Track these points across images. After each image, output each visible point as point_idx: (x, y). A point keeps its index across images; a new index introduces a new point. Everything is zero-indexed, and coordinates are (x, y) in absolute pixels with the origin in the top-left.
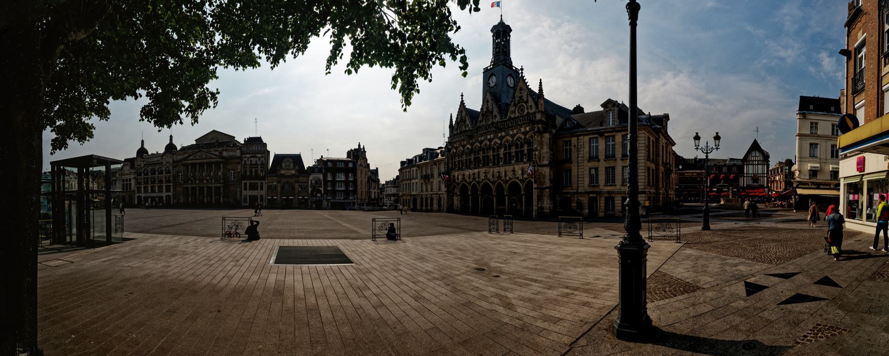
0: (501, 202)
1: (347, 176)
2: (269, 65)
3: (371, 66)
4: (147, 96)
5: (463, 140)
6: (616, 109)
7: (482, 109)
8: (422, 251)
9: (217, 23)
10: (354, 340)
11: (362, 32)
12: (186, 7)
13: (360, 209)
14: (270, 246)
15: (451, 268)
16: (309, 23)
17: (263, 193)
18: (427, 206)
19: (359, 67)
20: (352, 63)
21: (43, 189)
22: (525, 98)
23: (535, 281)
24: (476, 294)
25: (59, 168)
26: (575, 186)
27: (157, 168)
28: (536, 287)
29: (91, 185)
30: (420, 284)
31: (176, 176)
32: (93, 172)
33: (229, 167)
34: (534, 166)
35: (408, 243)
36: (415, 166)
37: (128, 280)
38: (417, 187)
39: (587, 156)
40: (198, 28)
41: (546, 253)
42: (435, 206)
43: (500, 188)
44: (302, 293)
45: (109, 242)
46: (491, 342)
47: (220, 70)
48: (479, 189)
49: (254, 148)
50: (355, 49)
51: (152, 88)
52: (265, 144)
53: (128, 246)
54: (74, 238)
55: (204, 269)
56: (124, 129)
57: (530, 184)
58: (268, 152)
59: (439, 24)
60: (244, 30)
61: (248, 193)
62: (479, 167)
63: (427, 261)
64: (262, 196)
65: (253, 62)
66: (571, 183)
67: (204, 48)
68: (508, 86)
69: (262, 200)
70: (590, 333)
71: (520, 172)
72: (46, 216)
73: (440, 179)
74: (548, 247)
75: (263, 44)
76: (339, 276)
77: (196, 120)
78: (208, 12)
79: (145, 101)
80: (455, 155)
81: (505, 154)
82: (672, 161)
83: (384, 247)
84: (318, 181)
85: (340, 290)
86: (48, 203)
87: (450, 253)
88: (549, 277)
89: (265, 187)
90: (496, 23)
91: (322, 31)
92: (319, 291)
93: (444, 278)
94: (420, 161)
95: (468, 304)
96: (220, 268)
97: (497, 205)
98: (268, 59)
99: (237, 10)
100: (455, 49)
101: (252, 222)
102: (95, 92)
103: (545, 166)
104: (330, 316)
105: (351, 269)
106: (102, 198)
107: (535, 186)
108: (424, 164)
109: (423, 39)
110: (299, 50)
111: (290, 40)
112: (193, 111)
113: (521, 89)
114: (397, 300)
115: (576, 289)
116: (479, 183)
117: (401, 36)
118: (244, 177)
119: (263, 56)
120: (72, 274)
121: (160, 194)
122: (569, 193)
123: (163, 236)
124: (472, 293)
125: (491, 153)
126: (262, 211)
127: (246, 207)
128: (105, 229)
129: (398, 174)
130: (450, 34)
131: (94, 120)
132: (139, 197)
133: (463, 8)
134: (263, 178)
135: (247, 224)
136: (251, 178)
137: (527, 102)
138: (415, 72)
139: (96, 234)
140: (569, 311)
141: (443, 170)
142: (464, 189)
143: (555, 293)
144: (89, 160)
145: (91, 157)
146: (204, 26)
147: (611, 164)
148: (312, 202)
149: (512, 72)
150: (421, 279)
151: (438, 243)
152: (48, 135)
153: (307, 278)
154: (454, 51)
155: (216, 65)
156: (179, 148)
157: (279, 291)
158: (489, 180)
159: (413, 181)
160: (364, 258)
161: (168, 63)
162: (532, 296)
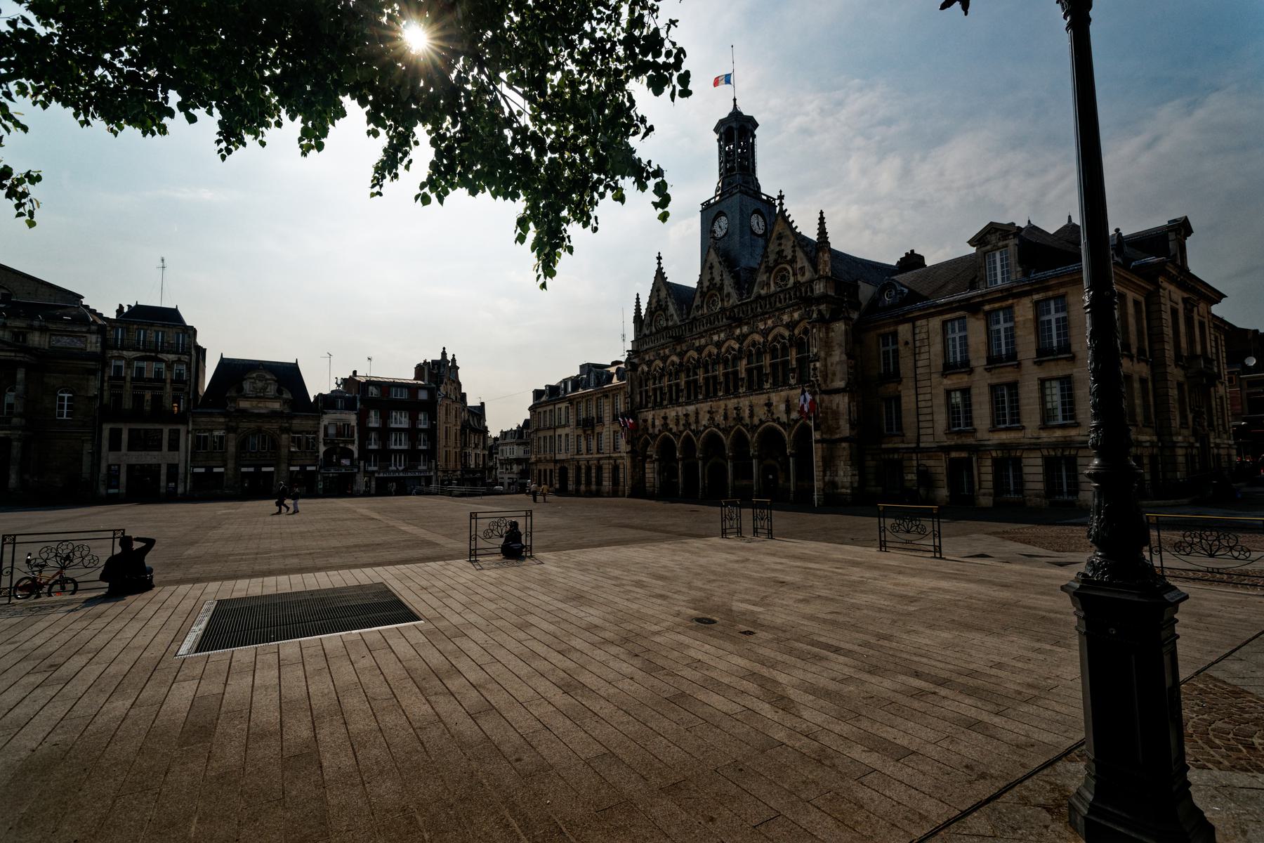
0: (743, 471)
1: (414, 420)
3: (473, 192)
5: (663, 347)
6: (1012, 242)
7: (700, 283)
8: (578, 580)
11: (454, 125)
14: (188, 605)
15: (642, 617)
17: (180, 457)
18: (588, 483)
19: (447, 193)
20: (431, 183)
22: (788, 253)
23: (837, 650)
24: (696, 676)
26: (910, 434)
28: (840, 666)
30: (575, 656)
34: (813, 394)
35: (550, 564)
36: (563, 400)
38: (567, 443)
39: (940, 362)
41: (856, 586)
42: (607, 484)
43: (740, 440)
46: (733, 790)
48: (699, 445)
49: (154, 335)
50: (439, 154)
57: (804, 433)
58: (201, 352)
59: (612, 122)
62: (697, 401)
63: (590, 603)
64: (173, 469)
66: (900, 428)
68: (753, 232)
70: (999, 805)
71: (782, 407)
73: (616, 427)
74: (856, 574)
80: (647, 376)
81: (749, 371)
82: (1213, 345)
83: (495, 575)
84: (344, 430)
85: (380, 690)
87: (639, 584)
88: (866, 644)
89: (185, 441)
90: (725, 115)
93: (627, 640)
94: (574, 389)
95: (679, 699)
97: (736, 477)
100: (643, 169)
101: (126, 542)
103: (837, 391)
104: (347, 762)
107: (816, 435)
108: (582, 396)
109: (581, 151)
113: (780, 237)
114: (524, 693)
115: (943, 683)
116: (697, 433)
117: (537, 141)
118: (113, 412)
122: (896, 450)
124: (688, 673)
125: (720, 371)
130: (633, 141)
133: (658, 91)
134: (181, 418)
135: (105, 550)
136: (137, 414)
137: (793, 261)
138: (565, 213)
140: (932, 735)
141: (621, 407)
142: (666, 447)
143: (887, 683)
147: (1007, 376)
149: (759, 205)
150: (577, 643)
151: (615, 564)
154: (641, 173)
158: (718, 426)
159: (559, 431)
160: (448, 601)
162: (833, 686)
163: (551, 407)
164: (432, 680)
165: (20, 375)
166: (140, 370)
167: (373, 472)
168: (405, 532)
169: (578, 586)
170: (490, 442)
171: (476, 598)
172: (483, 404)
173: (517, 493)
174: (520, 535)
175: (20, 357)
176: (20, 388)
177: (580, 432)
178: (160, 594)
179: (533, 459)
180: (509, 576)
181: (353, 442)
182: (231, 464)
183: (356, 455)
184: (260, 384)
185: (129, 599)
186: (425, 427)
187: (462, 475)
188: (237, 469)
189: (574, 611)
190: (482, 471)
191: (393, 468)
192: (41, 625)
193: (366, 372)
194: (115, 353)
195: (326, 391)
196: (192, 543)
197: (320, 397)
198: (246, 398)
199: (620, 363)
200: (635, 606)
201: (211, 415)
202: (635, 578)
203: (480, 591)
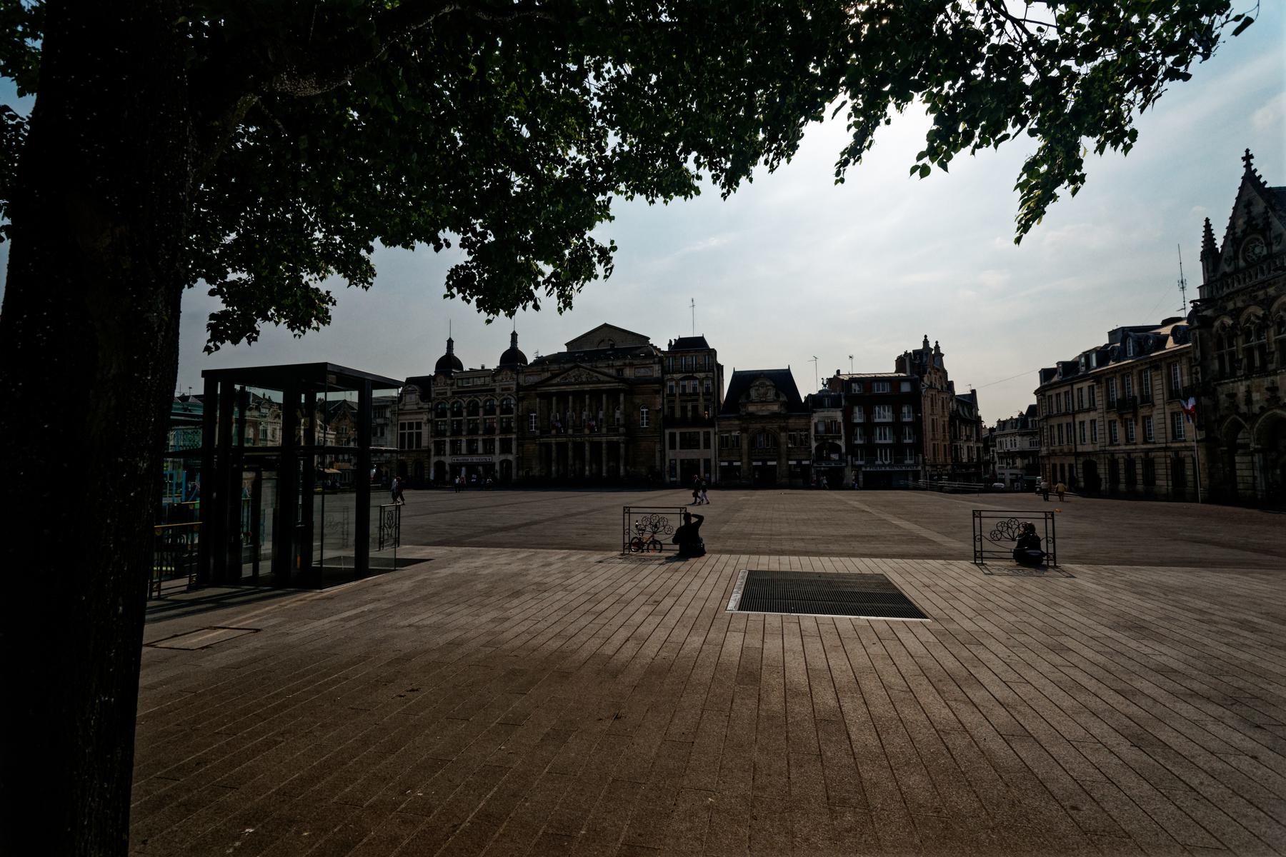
1: (897, 413)
2: (717, 189)
4: (461, 246)
9: (612, 112)
10: (938, 811)
12: (549, 77)
13: (930, 488)
14: (729, 570)
16: (800, 98)
17: (711, 453)
21: (174, 440)
25: (228, 388)
27: (481, 400)
29: (318, 435)
30: (1144, 702)
31: (523, 419)
32: (325, 403)
33: (638, 400)
36: (1085, 378)
37: (408, 658)
38: (1094, 430)
40: (572, 120)
42: (1163, 482)
44: (803, 679)
45: (361, 569)
47: (618, 203)
49: (690, 359)
51: (474, 231)
52: (714, 351)
53: (410, 577)
54: (266, 567)
55: (583, 622)
56: (403, 312)
58: (720, 368)
60: (665, 124)
61: (678, 454)
64: (707, 461)
65: (684, 186)
67: (584, 159)
69: (707, 469)
72: (180, 512)
75: (704, 150)
76: (892, 646)
77: (567, 302)
78: (593, 90)
79: (457, 255)
83: (1005, 583)
84: (831, 427)
86: (190, 477)
89: (714, 440)
91: (830, 108)
92: (843, 678)
93: (1236, 701)
94: (1099, 364)
96: (619, 620)
98: (715, 178)
99: (651, 87)
101: (688, 517)
102: (338, 221)
104: (872, 741)
105: (920, 631)
106: (346, 466)
108: (1114, 370)
110: (778, 155)
111: (761, 136)
112: (563, 283)
114: (1070, 729)
118: (670, 421)
119: (706, 173)
120: (255, 660)
121: (488, 458)
123: (492, 551)
126: (710, 493)
127: (673, 486)
128: (352, 539)
129: (1033, 400)
131: (333, 283)
132: (440, 465)
134: (710, 423)
135: (676, 522)
136: (684, 422)
139: (328, 554)
144: (320, 375)
145: (322, 368)
146: (586, 117)
148: (819, 473)
152: (199, 302)
153: (814, 646)
155: (610, 194)
156: (530, 360)
157: (750, 673)
159: (1079, 418)
161: (509, 184)
163: (1067, 388)
164: (957, 683)
165: (622, 398)
166: (684, 387)
167: (861, 466)
168: (897, 527)
169: (1134, 613)
170: (985, 434)
171: (989, 605)
172: (974, 392)
173: (1023, 491)
174: (1038, 540)
175: (621, 386)
176: (622, 407)
177: (1114, 416)
178: (710, 559)
179: (1044, 450)
180: (1028, 586)
181: (840, 438)
182: (745, 460)
183: (844, 450)
184: (762, 391)
185: (692, 560)
186: (910, 420)
187: (953, 469)
188: (750, 463)
189: (1133, 644)
190: (977, 466)
191: (879, 462)
192: (646, 572)
193: (849, 369)
194: (669, 376)
195: (815, 392)
196: (726, 522)
197: (810, 397)
198: (752, 402)
199: (1180, 319)
200: (1247, 657)
201: (729, 419)
202: (1238, 616)
203: (993, 598)
